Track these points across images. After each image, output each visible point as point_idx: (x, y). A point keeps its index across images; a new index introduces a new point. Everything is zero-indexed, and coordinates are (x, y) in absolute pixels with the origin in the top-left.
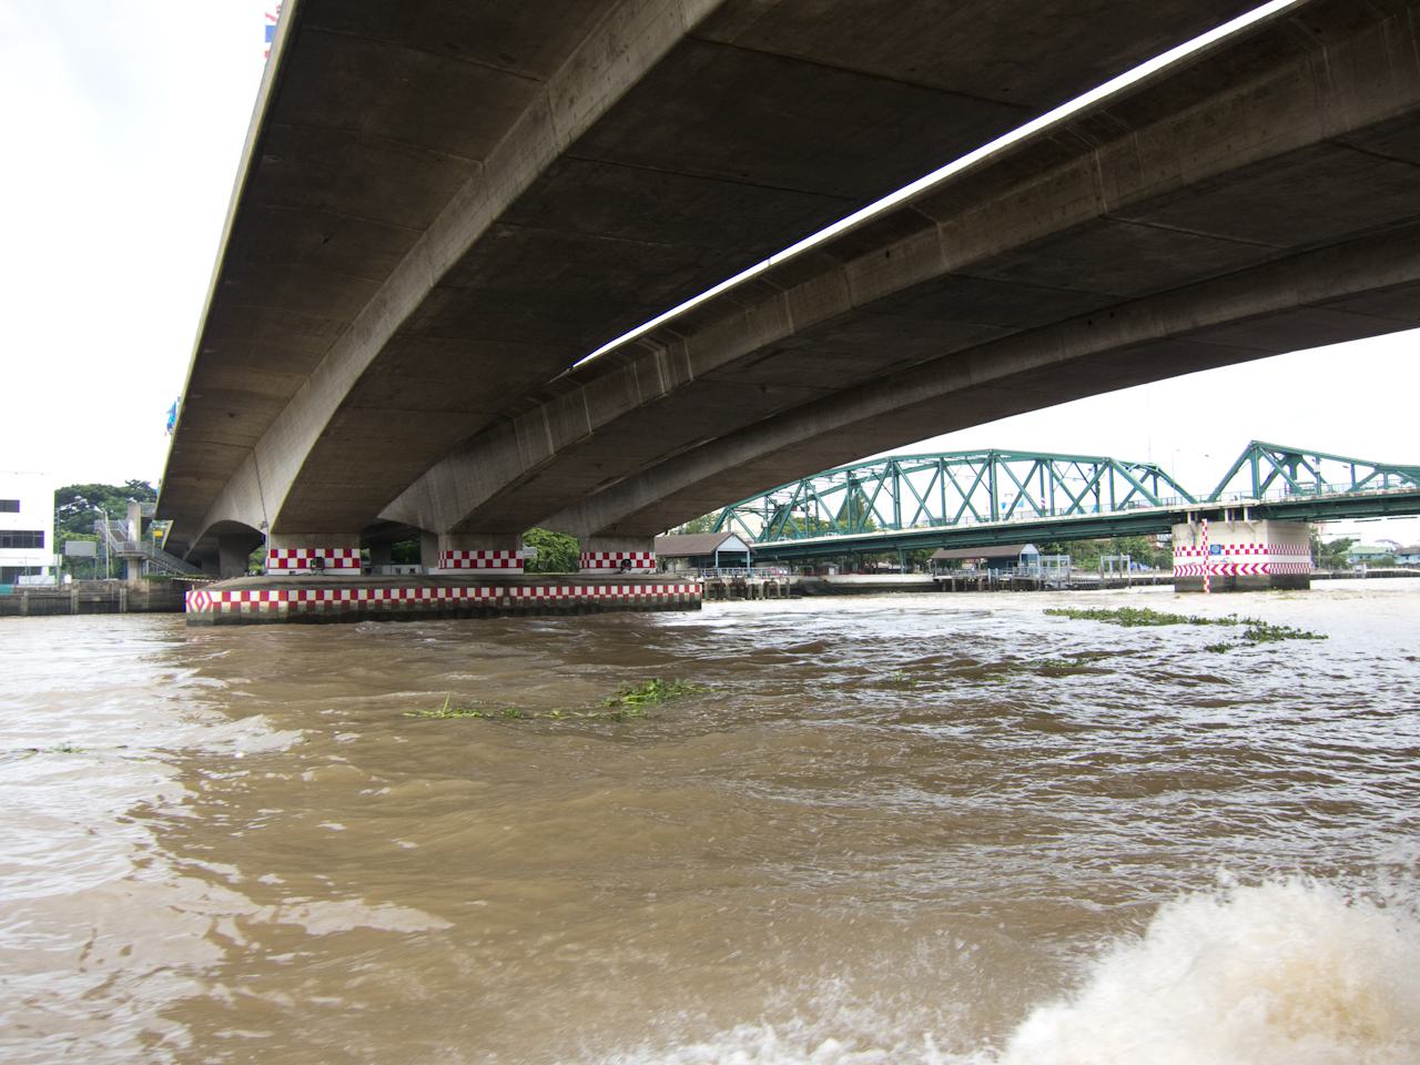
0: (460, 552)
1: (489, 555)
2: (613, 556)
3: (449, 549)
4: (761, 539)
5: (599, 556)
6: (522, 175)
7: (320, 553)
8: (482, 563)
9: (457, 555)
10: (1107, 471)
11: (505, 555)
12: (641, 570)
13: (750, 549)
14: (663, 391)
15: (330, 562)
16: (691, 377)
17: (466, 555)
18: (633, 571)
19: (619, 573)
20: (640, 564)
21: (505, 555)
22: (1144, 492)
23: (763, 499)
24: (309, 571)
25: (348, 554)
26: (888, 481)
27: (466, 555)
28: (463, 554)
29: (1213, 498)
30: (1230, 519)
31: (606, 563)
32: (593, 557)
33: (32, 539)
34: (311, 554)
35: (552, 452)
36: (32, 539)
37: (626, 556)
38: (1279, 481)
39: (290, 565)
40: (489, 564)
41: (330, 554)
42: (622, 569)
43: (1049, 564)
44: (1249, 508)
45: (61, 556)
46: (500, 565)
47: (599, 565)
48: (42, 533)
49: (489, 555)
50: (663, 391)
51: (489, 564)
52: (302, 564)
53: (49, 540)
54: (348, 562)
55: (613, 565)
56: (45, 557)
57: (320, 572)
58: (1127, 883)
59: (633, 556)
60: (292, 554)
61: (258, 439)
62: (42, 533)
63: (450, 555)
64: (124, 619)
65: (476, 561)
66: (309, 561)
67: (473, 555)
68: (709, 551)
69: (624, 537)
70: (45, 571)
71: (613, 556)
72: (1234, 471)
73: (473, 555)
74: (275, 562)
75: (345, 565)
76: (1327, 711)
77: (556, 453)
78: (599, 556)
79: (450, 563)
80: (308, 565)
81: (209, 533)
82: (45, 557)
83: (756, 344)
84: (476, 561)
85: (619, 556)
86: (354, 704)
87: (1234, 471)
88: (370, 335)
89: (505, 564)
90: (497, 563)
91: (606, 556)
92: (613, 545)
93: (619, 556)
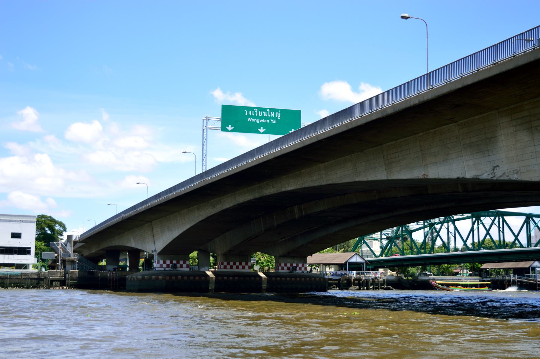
0: (226, 262)
1: (238, 264)
2: (289, 265)
3: (222, 261)
4: (381, 255)
5: (283, 265)
6: (257, 195)
7: (175, 262)
8: (234, 267)
9: (225, 263)
11: (244, 264)
12: (300, 271)
13: (366, 261)
14: (297, 217)
15: (178, 265)
16: (304, 215)
17: (228, 264)
18: (297, 271)
19: (291, 272)
20: (300, 269)
21: (244, 264)
23: (379, 233)
24: (171, 269)
26: (445, 224)
27: (228, 264)
28: (234, 263)
31: (286, 268)
32: (280, 265)
33: (25, 251)
34: (171, 262)
35: (263, 230)
36: (25, 251)
37: (294, 265)
39: (164, 266)
40: (238, 268)
41: (178, 262)
42: (292, 271)
45: (374, 278)
47: (283, 269)
48: (30, 248)
49: (238, 264)
50: (297, 217)
51: (238, 268)
52: (168, 266)
53: (33, 251)
54: (185, 266)
55: (289, 269)
56: (30, 259)
57: (175, 269)
59: (297, 265)
60: (165, 262)
62: (30, 248)
63: (222, 264)
64: (6, 291)
66: (171, 265)
67: (231, 264)
68: (344, 262)
69: (294, 257)
70: (31, 267)
71: (289, 265)
73: (231, 264)
74: (158, 265)
75: (184, 267)
77: (264, 230)
78: (283, 265)
79: (222, 267)
80: (170, 266)
81: (103, 249)
82: (30, 259)
83: (319, 210)
85: (291, 265)
88: (215, 207)
89: (244, 268)
90: (241, 267)
91: (286, 265)
92: (289, 260)
93: (291, 265)
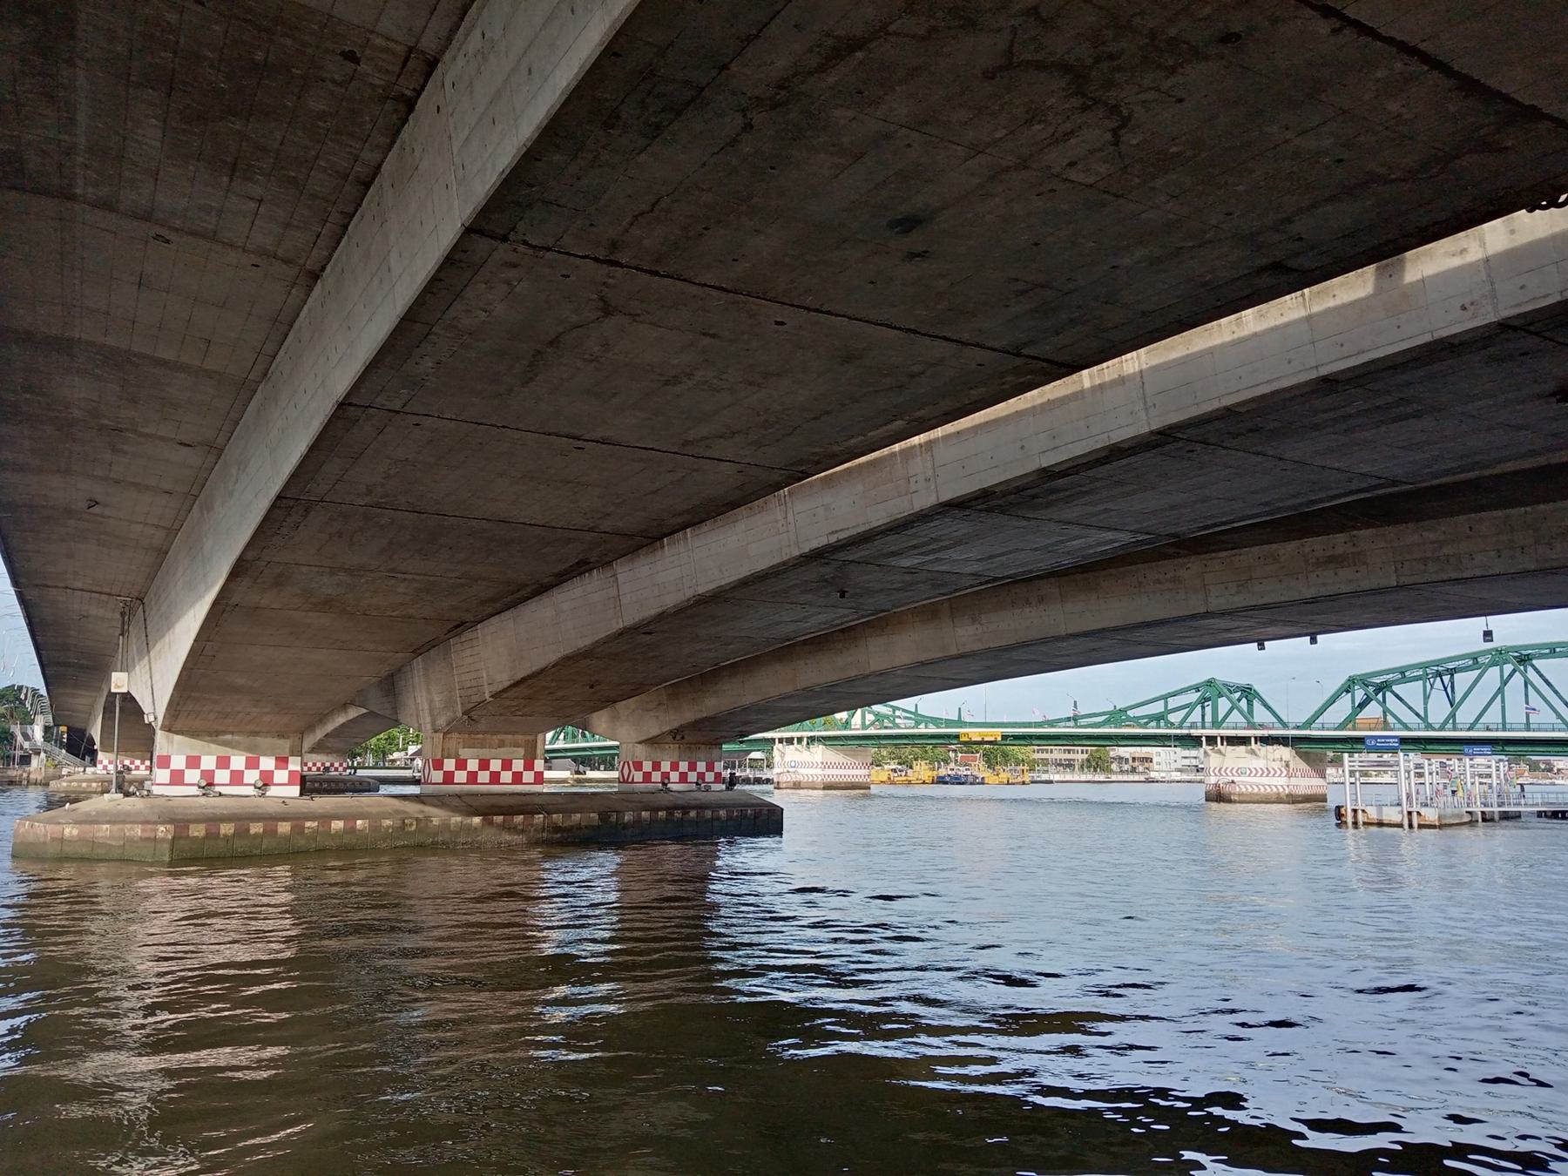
1: (238, 761)
10: (1388, 694)
22: (1241, 712)
25: (143, 763)
29: (1308, 724)
30: (1222, 744)
37: (328, 764)
38: (1236, 717)
43: (1421, 780)
44: (808, 738)
46: (713, 779)
54: (143, 767)
58: (93, 1010)
61: (172, 532)
65: (181, 773)
72: (1526, 695)
75: (245, 781)
76: (761, 890)
84: (181, 773)
86: (382, 1021)
87: (1526, 695)
